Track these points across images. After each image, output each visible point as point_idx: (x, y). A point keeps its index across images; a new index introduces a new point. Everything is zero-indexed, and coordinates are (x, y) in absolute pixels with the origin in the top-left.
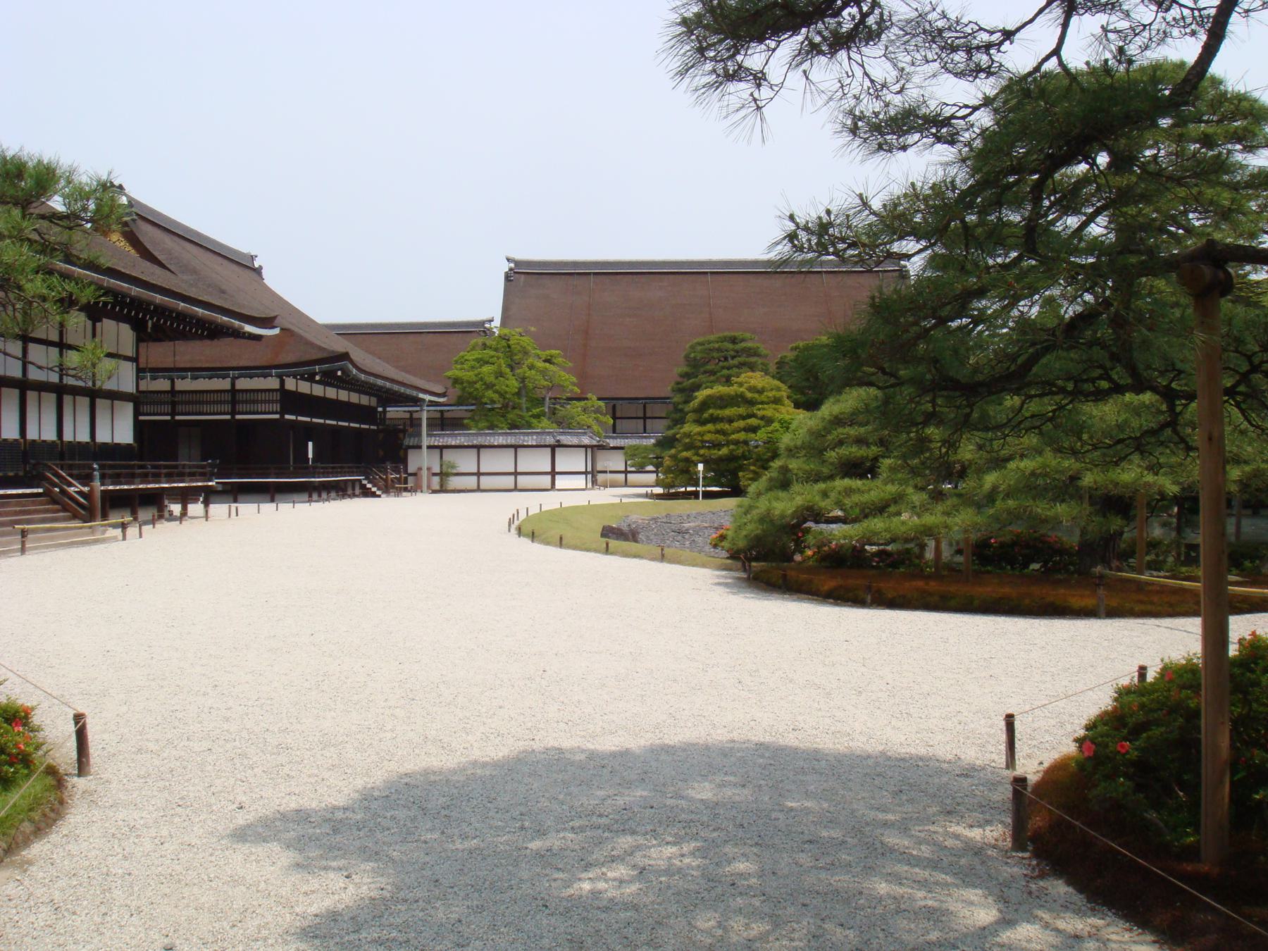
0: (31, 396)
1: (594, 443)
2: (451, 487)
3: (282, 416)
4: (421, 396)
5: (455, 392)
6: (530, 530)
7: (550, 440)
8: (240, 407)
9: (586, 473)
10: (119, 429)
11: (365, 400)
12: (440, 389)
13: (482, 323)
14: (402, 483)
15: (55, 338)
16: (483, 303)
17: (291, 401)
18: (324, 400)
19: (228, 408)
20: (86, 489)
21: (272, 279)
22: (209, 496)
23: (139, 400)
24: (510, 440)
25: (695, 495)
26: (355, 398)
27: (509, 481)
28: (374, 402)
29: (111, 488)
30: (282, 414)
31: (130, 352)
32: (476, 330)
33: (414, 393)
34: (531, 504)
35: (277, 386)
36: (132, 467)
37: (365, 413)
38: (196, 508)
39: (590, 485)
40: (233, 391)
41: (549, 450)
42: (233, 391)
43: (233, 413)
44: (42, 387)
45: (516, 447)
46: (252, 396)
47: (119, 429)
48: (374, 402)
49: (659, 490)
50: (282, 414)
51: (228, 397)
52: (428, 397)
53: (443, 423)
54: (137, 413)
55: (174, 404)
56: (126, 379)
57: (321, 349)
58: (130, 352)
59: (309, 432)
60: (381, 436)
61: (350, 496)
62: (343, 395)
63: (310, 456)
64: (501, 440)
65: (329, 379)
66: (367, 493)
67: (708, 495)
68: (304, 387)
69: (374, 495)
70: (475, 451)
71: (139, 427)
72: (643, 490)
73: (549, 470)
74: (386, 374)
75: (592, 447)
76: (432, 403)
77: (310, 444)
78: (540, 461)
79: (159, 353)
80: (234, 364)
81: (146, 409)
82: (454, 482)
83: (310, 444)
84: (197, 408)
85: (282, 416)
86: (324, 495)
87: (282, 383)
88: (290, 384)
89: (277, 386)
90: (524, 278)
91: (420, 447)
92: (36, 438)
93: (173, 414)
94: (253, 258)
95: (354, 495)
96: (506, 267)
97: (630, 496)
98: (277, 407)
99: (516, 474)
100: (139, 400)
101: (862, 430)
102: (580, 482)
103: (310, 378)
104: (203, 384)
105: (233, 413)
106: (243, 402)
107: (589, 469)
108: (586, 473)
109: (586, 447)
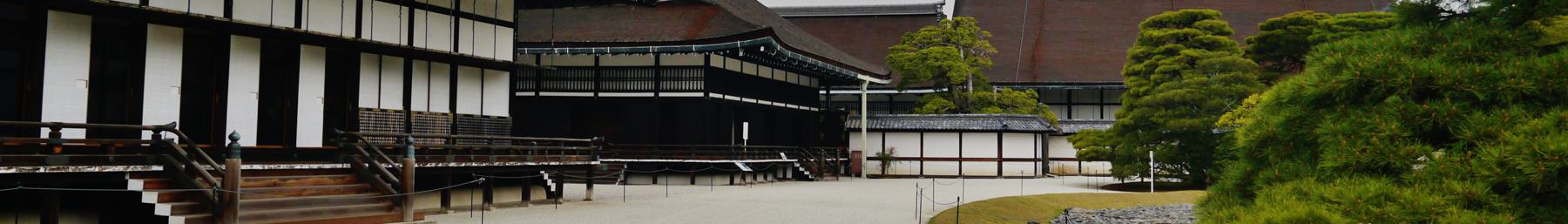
0: (417, 66)
2: (890, 171)
4: (860, 76)
5: (898, 76)
7: (999, 126)
8: (603, 85)
9: (1035, 160)
10: (495, 101)
11: (804, 81)
12: (883, 72)
14: (850, 168)
17: (716, 79)
18: (771, 82)
19: (651, 85)
20: (399, 165)
22: (590, 177)
24: (957, 124)
25: (1143, 187)
27: (953, 168)
28: (815, 83)
29: (452, 164)
33: (852, 74)
35: (702, 63)
37: (808, 95)
39: (1040, 172)
40: (657, 67)
41: (995, 136)
42: (657, 67)
43: (596, 91)
45: (961, 132)
48: (815, 83)
49: (1111, 180)
51: (592, 74)
52: (868, 79)
53: (885, 106)
54: (513, 90)
59: (743, 112)
60: (822, 119)
61: (780, 180)
62: (779, 75)
63: (745, 137)
65: (752, 55)
66: (799, 177)
67: (1160, 187)
68: (733, 65)
69: (806, 179)
70: (957, 136)
71: (514, 102)
72: (1101, 180)
73: (995, 155)
74: (830, 56)
78: (985, 146)
80: (653, 39)
82: (896, 167)
84: (676, 85)
86: (760, 178)
87: (707, 59)
88: (716, 61)
89: (702, 63)
91: (859, 130)
92: (424, 109)
93: (596, 91)
95: (784, 179)
98: (701, 85)
99: (960, 159)
102: (1029, 168)
103: (733, 54)
104: (569, 60)
105: (657, 91)
107: (1039, 155)
108: (1035, 160)
109: (1035, 132)
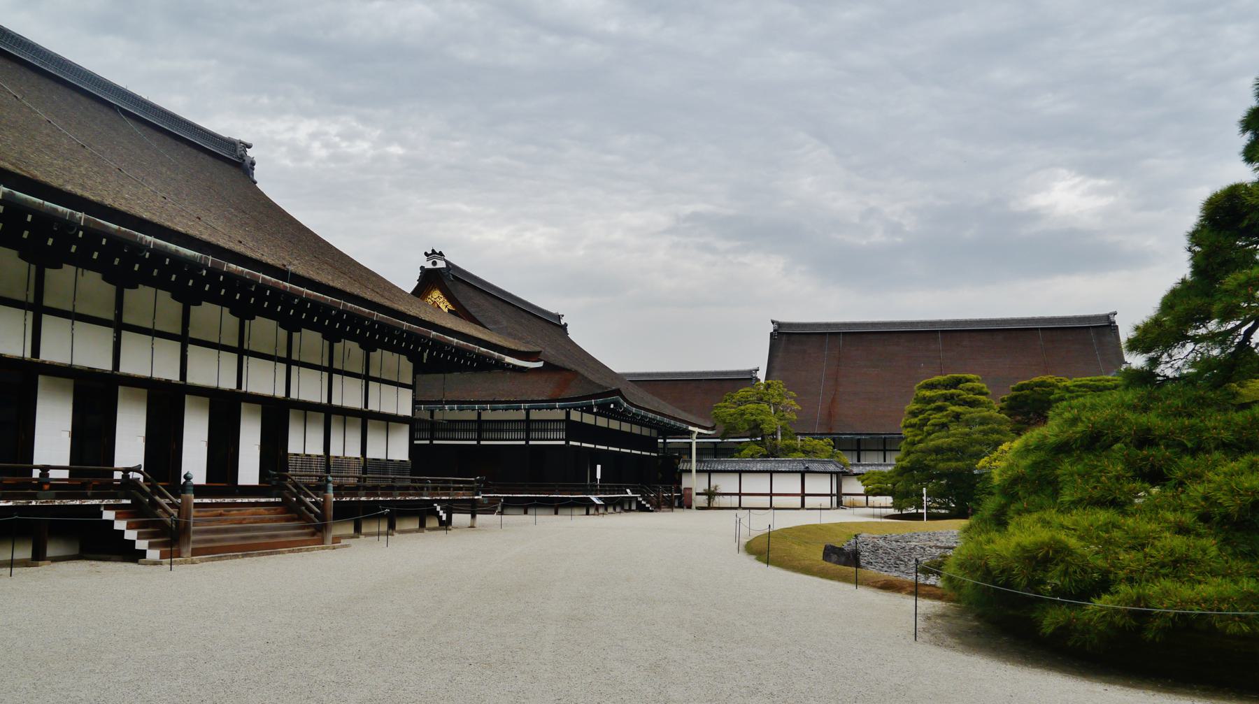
1: (838, 470)
3: (567, 443)
4: (691, 428)
5: (721, 428)
6: (765, 550)
9: (831, 495)
10: (397, 448)
11: (646, 432)
13: (750, 372)
14: (682, 502)
15: (326, 364)
16: (754, 357)
17: (576, 430)
19: (475, 435)
21: (573, 334)
22: (474, 509)
23: (411, 423)
24: (769, 466)
25: (918, 517)
26: (636, 429)
27: (765, 501)
30: (567, 441)
31: (410, 382)
32: (747, 378)
33: (684, 426)
34: (759, 524)
36: (448, 481)
37: (649, 443)
38: (460, 519)
39: (835, 505)
41: (799, 476)
42: (528, 421)
43: (527, 440)
44: (346, 413)
45: (771, 472)
46: (540, 426)
47: (397, 448)
49: (892, 511)
50: (567, 441)
52: (697, 430)
55: (528, 431)
56: (400, 403)
57: (600, 386)
58: (410, 382)
59: (596, 457)
61: (626, 511)
63: (599, 476)
64: (759, 467)
65: (604, 411)
66: (641, 508)
67: (931, 517)
68: (589, 419)
70: (768, 475)
71: (413, 449)
75: (837, 473)
76: (700, 436)
77: (599, 467)
78: (791, 484)
79: (435, 384)
81: (533, 435)
82: (719, 501)
83: (599, 467)
84: (542, 435)
85: (567, 443)
87: (568, 414)
88: (575, 416)
90: (788, 340)
91: (690, 471)
94: (559, 317)
95: (630, 510)
96: (771, 328)
97: (866, 516)
98: (562, 435)
99: (771, 495)
100: (411, 423)
101: (960, 464)
102: (826, 501)
103: (589, 410)
105: (527, 440)
106: (535, 430)
107: (835, 492)
108: (831, 495)
109: (831, 473)
